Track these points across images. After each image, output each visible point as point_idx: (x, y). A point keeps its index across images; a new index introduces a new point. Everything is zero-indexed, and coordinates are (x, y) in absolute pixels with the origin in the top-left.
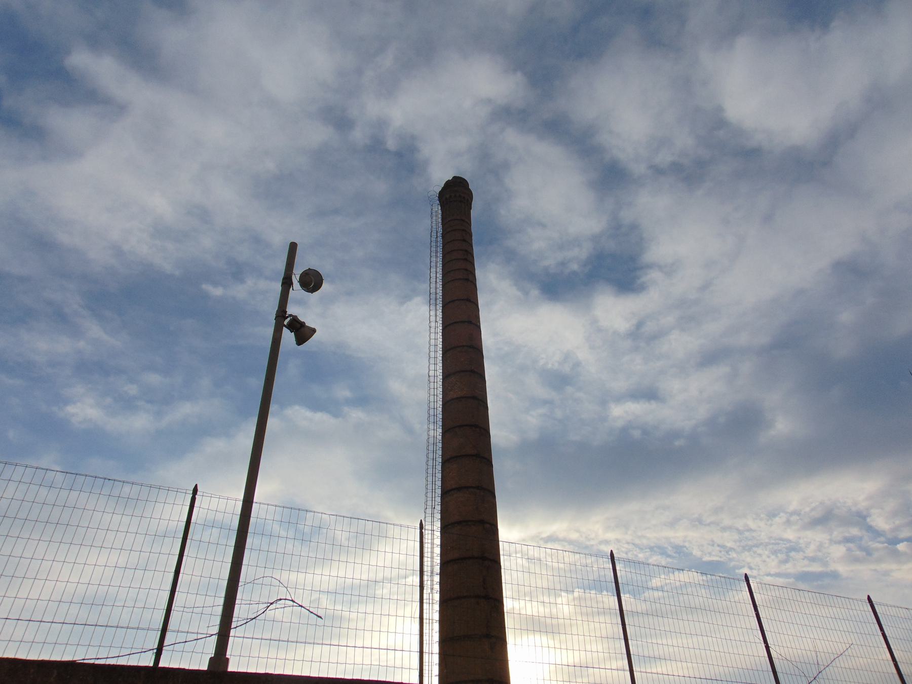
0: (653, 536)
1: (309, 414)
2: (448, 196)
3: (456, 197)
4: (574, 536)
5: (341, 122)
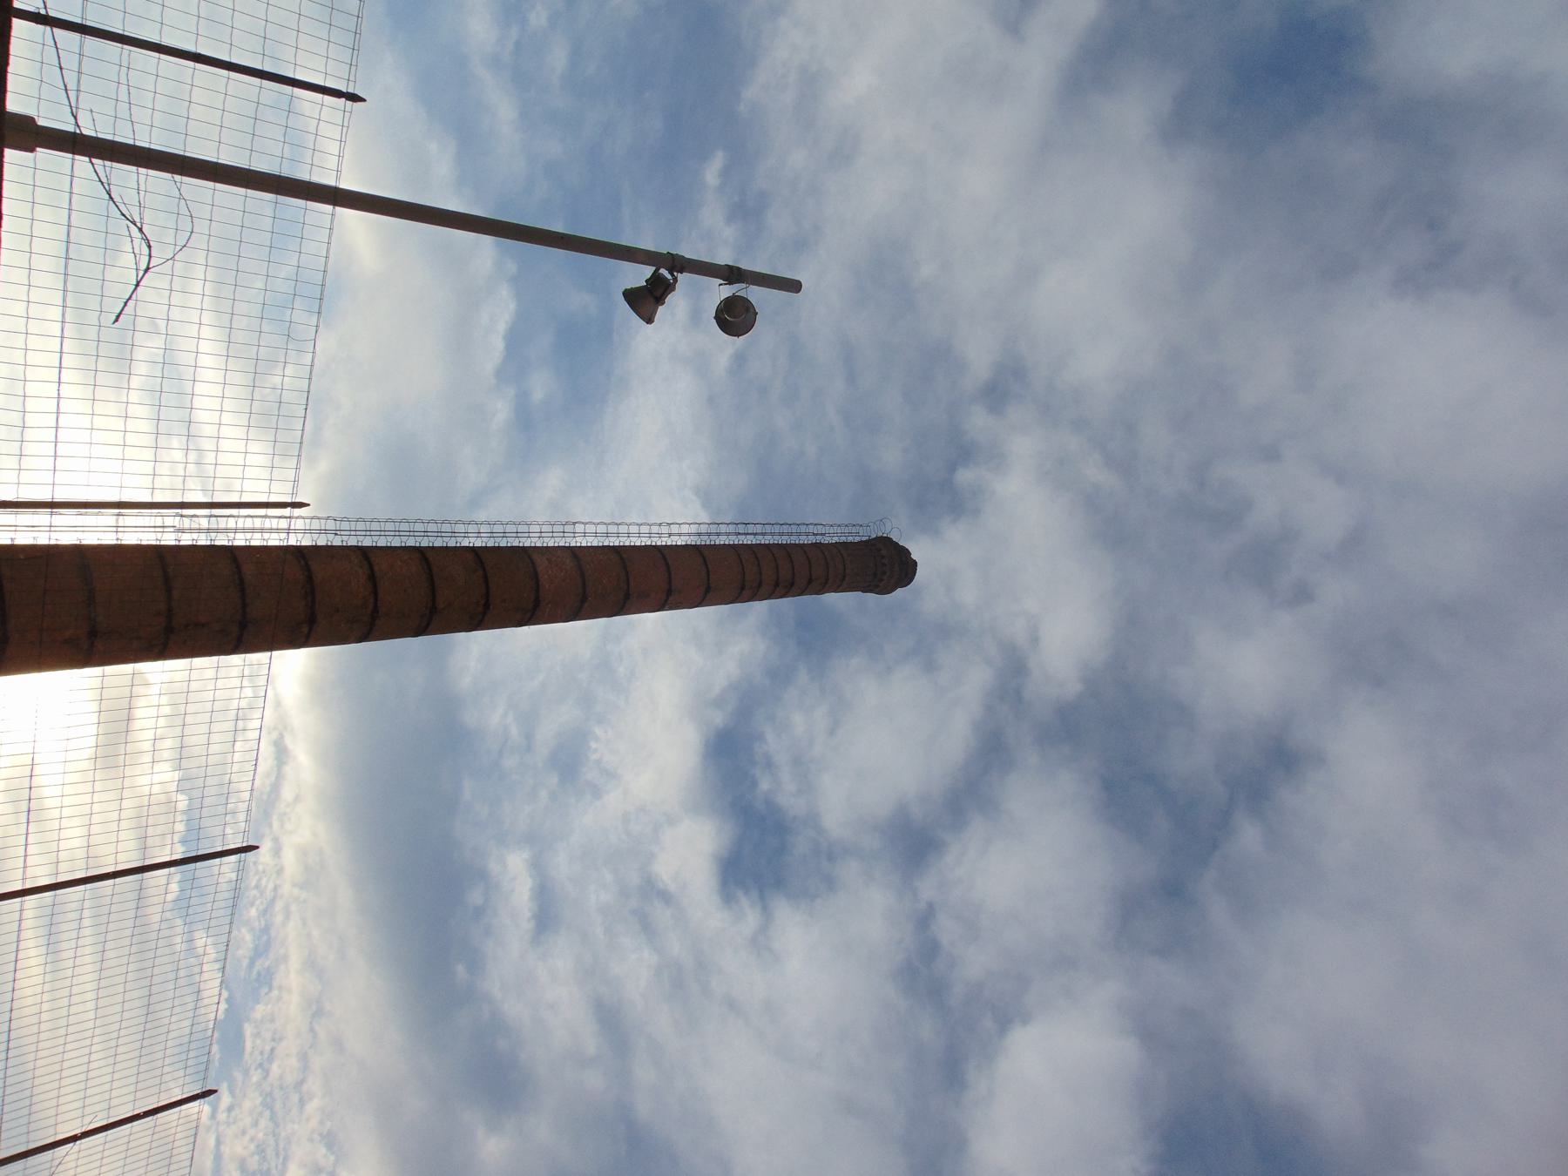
0: (292, 937)
1: (502, 326)
2: (884, 552)
3: (881, 566)
4: (287, 793)
5: (998, 392)
